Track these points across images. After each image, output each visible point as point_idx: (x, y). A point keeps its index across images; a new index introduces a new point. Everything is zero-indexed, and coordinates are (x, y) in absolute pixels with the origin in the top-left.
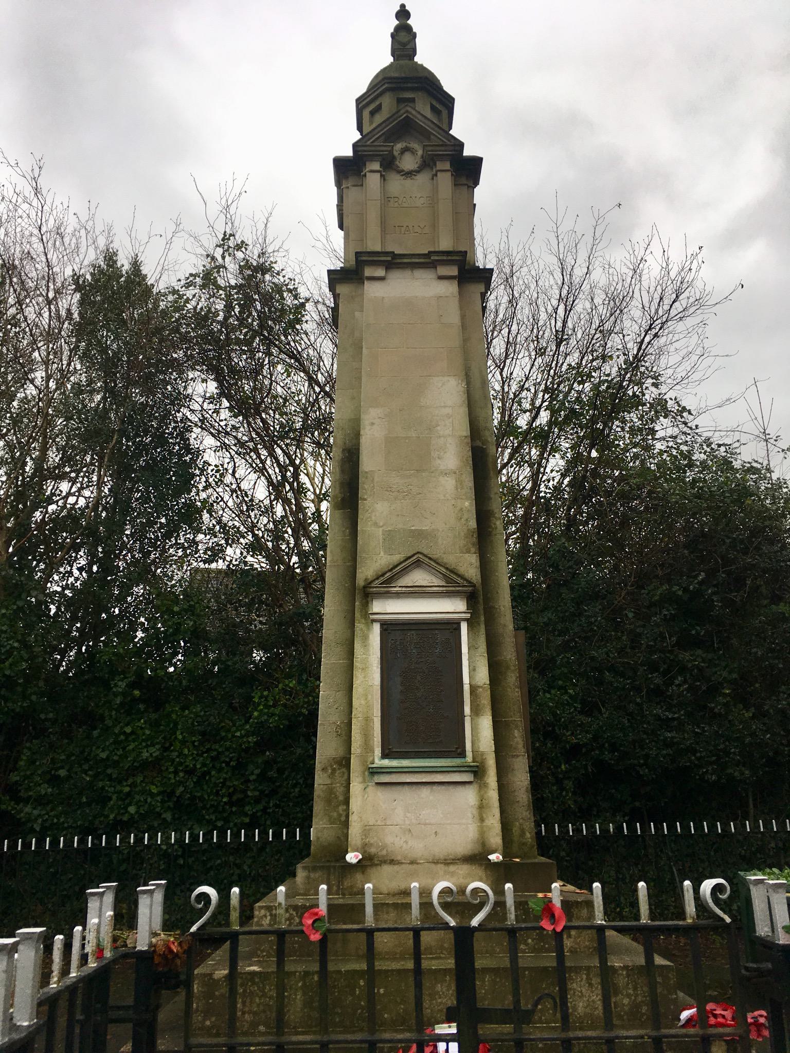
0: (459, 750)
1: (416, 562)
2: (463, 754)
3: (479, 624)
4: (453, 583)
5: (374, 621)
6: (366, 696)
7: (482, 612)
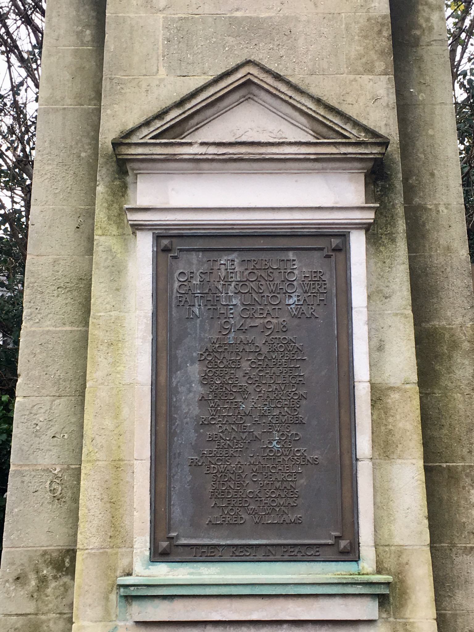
0: (343, 544)
1: (243, 86)
2: (351, 553)
3: (393, 240)
4: (332, 137)
5: (137, 227)
6: (115, 410)
7: (400, 211)
